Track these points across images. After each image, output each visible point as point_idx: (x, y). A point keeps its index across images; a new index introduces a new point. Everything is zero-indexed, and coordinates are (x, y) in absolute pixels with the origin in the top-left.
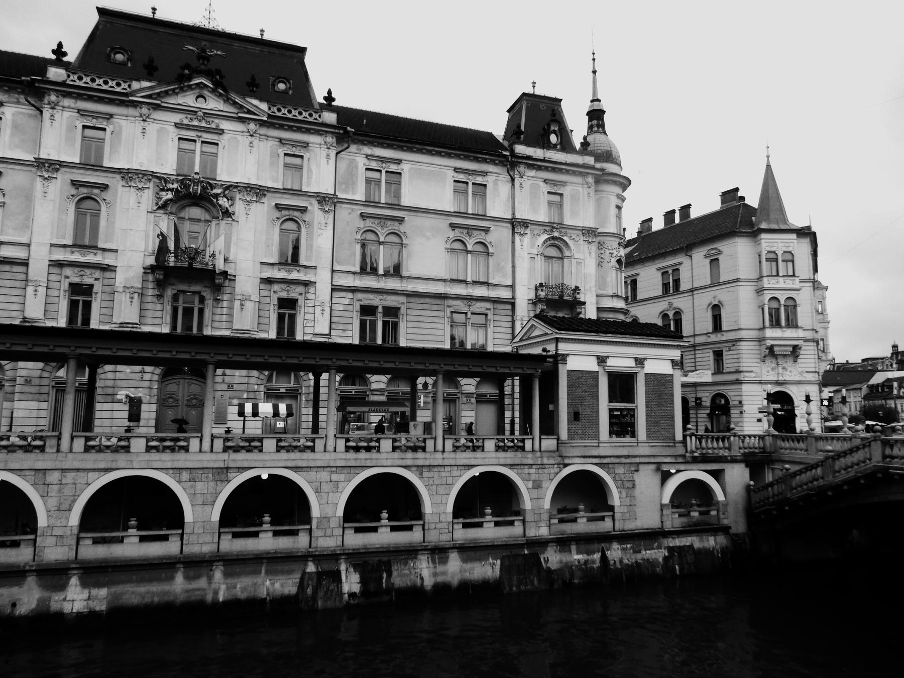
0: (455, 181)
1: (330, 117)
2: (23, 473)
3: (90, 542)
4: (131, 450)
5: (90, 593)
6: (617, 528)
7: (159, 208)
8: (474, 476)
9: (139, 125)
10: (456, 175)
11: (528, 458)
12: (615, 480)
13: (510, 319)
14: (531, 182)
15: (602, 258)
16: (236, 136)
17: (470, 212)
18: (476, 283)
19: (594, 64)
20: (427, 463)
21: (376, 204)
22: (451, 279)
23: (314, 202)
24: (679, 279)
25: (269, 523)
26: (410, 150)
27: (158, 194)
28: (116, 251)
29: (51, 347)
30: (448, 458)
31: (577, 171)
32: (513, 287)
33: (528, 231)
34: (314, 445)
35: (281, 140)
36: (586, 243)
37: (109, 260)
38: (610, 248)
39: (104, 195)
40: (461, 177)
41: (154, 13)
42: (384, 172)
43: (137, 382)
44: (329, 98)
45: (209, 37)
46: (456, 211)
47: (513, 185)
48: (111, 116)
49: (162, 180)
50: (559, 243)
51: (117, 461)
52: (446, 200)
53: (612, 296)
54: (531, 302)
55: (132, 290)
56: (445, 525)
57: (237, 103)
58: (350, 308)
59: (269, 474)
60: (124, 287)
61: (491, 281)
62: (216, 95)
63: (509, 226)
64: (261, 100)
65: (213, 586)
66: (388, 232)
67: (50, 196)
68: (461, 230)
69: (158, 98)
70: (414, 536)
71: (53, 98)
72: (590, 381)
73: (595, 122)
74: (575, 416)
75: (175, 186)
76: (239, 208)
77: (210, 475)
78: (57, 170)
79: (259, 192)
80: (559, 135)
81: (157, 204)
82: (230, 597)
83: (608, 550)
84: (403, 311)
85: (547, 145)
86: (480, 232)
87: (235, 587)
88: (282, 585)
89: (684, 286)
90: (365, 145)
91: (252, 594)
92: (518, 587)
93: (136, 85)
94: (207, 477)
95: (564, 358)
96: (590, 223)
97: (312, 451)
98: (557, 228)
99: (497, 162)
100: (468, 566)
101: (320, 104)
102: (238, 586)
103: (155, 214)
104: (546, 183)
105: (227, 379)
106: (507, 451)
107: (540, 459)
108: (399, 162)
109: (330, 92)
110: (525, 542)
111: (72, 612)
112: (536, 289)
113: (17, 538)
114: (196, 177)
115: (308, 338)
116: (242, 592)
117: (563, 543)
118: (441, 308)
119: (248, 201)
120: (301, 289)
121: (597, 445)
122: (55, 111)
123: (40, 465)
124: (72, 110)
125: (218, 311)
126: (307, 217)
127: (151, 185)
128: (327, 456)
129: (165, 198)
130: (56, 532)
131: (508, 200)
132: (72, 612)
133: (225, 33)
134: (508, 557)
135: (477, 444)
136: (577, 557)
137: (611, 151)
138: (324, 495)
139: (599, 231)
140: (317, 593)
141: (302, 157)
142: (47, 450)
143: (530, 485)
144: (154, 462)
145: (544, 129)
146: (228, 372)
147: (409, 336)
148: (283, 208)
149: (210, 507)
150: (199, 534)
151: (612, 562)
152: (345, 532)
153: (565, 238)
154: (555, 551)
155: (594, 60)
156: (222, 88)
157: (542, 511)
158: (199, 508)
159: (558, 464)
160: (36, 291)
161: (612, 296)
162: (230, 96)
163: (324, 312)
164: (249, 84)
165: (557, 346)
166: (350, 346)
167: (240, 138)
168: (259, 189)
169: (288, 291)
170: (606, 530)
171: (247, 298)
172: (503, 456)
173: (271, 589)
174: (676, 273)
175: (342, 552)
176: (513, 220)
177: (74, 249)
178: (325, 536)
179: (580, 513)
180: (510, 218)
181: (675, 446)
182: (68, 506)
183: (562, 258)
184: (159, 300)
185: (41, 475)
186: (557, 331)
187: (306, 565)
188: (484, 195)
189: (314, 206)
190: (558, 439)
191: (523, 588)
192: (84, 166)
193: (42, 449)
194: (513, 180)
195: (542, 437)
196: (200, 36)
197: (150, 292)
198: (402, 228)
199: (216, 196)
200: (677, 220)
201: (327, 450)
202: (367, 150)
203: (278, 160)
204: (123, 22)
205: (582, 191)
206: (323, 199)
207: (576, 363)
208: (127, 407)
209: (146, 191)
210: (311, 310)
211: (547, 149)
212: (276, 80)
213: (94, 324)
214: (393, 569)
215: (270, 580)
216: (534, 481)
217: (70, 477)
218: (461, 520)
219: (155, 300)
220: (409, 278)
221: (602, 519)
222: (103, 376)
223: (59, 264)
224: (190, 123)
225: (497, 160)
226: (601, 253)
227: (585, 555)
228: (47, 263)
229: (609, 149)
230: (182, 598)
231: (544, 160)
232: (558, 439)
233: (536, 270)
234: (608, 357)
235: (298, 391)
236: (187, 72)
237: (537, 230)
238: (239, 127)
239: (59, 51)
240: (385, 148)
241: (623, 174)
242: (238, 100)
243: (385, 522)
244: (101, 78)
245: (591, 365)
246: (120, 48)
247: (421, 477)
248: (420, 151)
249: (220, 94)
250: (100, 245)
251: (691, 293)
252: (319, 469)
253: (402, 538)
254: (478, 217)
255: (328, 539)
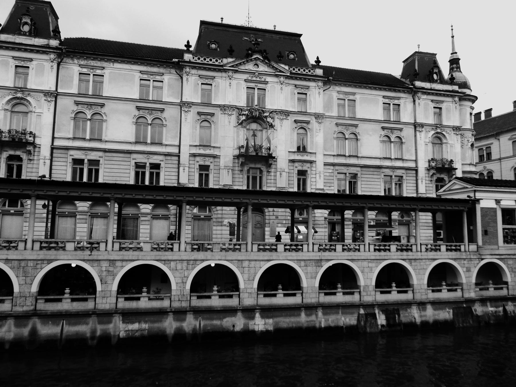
0: (384, 103)
1: (319, 72)
2: (233, 262)
3: (262, 296)
4: (278, 251)
5: (265, 321)
6: (510, 294)
7: (239, 124)
8: (330, 266)
9: (228, 81)
10: (384, 100)
11: (463, 255)
12: (508, 268)
13: (415, 178)
14: (424, 102)
15: (463, 143)
16: (274, 85)
17: (392, 120)
18: (396, 159)
19: (452, 32)
20: (414, 258)
21: (343, 118)
22: (383, 158)
23: (313, 118)
24: (491, 153)
25: (69, 294)
26: (360, 87)
27: (238, 117)
28: (220, 148)
29: (68, 193)
30: (424, 255)
31: (450, 94)
32: (416, 161)
33: (423, 129)
34: (241, 248)
35: (296, 86)
36: (455, 135)
37: (216, 152)
38: (467, 137)
39: (213, 119)
40: (387, 101)
41: (222, 21)
42: (391, 105)
43: (233, 215)
44: (318, 61)
45: (254, 32)
46: (299, 111)
47: (414, 104)
48: (214, 77)
49: (240, 109)
50: (440, 136)
51: (272, 256)
52: (379, 114)
53: (470, 164)
54: (426, 169)
55: (228, 168)
56: (423, 291)
57: (275, 67)
58: (332, 174)
59: (76, 265)
60: (224, 166)
61: (404, 158)
62: (264, 64)
63: (413, 127)
64: (285, 65)
65: (319, 319)
66: (350, 133)
67: (188, 120)
68: (387, 130)
69: (237, 67)
70: (409, 296)
71: (188, 70)
72: (492, 213)
73: (455, 66)
74: (485, 233)
75: (247, 112)
76: (277, 123)
77: (314, 263)
78: (191, 107)
79: (286, 114)
80: (438, 74)
81: (238, 122)
82: (327, 325)
83: (506, 306)
84: (359, 175)
85: (432, 81)
86: (398, 131)
87: (328, 320)
88: (350, 320)
89: (494, 156)
90: (337, 85)
91: (336, 325)
92: (463, 324)
93: (225, 61)
94: (312, 264)
95: (478, 201)
96: (457, 124)
97: (171, 251)
98: (439, 127)
99: (406, 91)
100: (437, 312)
101: (312, 65)
102: (330, 320)
103: (237, 128)
104: (433, 102)
105: (275, 213)
106: (331, 251)
107: (469, 256)
108: (354, 94)
109: (318, 58)
110: (464, 300)
111: (259, 330)
112: (429, 162)
113: (231, 293)
114: (256, 107)
115: (313, 191)
116: (332, 323)
117: (483, 301)
118: (379, 173)
119: (281, 119)
120: (308, 165)
121: (497, 248)
122: (188, 76)
123: (240, 258)
124: (196, 75)
125: (269, 177)
126: (310, 126)
127: (234, 113)
128: (309, 254)
129: (242, 120)
130: (249, 291)
131: (412, 113)
132: (259, 330)
133: (257, 28)
134: (456, 308)
135: (350, 247)
136: (491, 309)
137: (466, 82)
138: (366, 274)
139: (462, 128)
140: (366, 324)
141: (211, 85)
142: (242, 250)
143: (465, 269)
144: (288, 257)
145: (430, 72)
146: (275, 209)
147: (363, 189)
148: (298, 122)
149: (314, 279)
150: (310, 293)
151: (509, 312)
152: (191, 298)
153: (443, 133)
154: (479, 306)
155: (452, 30)
156: (267, 59)
157: (471, 284)
158: (309, 280)
159: (478, 259)
160: (184, 169)
161: (470, 164)
162: (271, 64)
163: (185, 170)
164: (278, 57)
165: (475, 194)
166: (334, 194)
167: (276, 85)
168: (286, 112)
169: (302, 166)
170: (504, 295)
171: (283, 170)
172: (451, 254)
173: (345, 322)
174: (488, 149)
175: (376, 304)
176: (416, 124)
177: (200, 147)
178: (367, 295)
179: (444, 287)
180: (413, 122)
181: (498, 249)
182: (253, 278)
183: (441, 144)
184: (241, 173)
185: (240, 263)
186: (475, 186)
187: (359, 310)
188: (354, 106)
189: (313, 120)
190: (477, 245)
191: (465, 325)
192: (203, 104)
193: (240, 250)
194: (414, 101)
195: (470, 244)
196: (249, 32)
197: (237, 168)
198: (357, 130)
199: (266, 117)
200: (483, 118)
201: (365, 251)
202: (338, 88)
203: (295, 96)
204: (213, 27)
205: (452, 106)
206: (318, 116)
207: (483, 204)
208: (228, 228)
209: (233, 116)
210: (314, 176)
211: (432, 83)
212: (289, 53)
213: (101, 180)
214: (400, 313)
215: (344, 317)
216: (467, 268)
217: (253, 264)
218: (431, 288)
219: (239, 172)
220: (362, 157)
221: (502, 288)
222: (216, 212)
223: (194, 155)
224: (252, 79)
225: (406, 90)
226: (462, 140)
227: (495, 308)
228: (189, 155)
229: (465, 81)
230: (305, 325)
231: (431, 89)
232: (477, 245)
233: (429, 151)
234: (501, 200)
235: (211, 217)
236: (250, 52)
237: (428, 128)
238: (275, 79)
239: (188, 46)
240: (347, 87)
241: (472, 94)
242: (275, 65)
243: (394, 288)
244: (208, 58)
245: (492, 204)
246: (214, 41)
247: (411, 264)
248: (365, 88)
249: (266, 63)
250: (212, 145)
251: (499, 161)
252: (363, 261)
253: (403, 297)
254: (99, 97)
255: (368, 296)
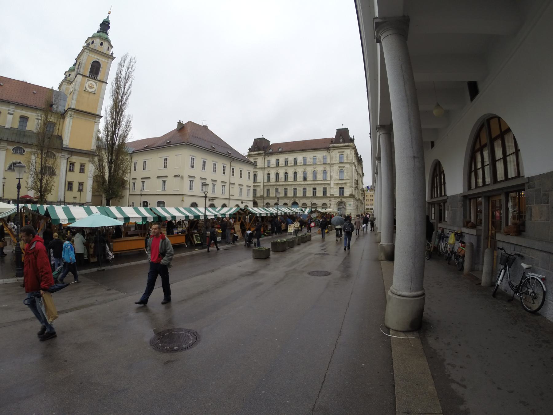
48: (344, 152)
